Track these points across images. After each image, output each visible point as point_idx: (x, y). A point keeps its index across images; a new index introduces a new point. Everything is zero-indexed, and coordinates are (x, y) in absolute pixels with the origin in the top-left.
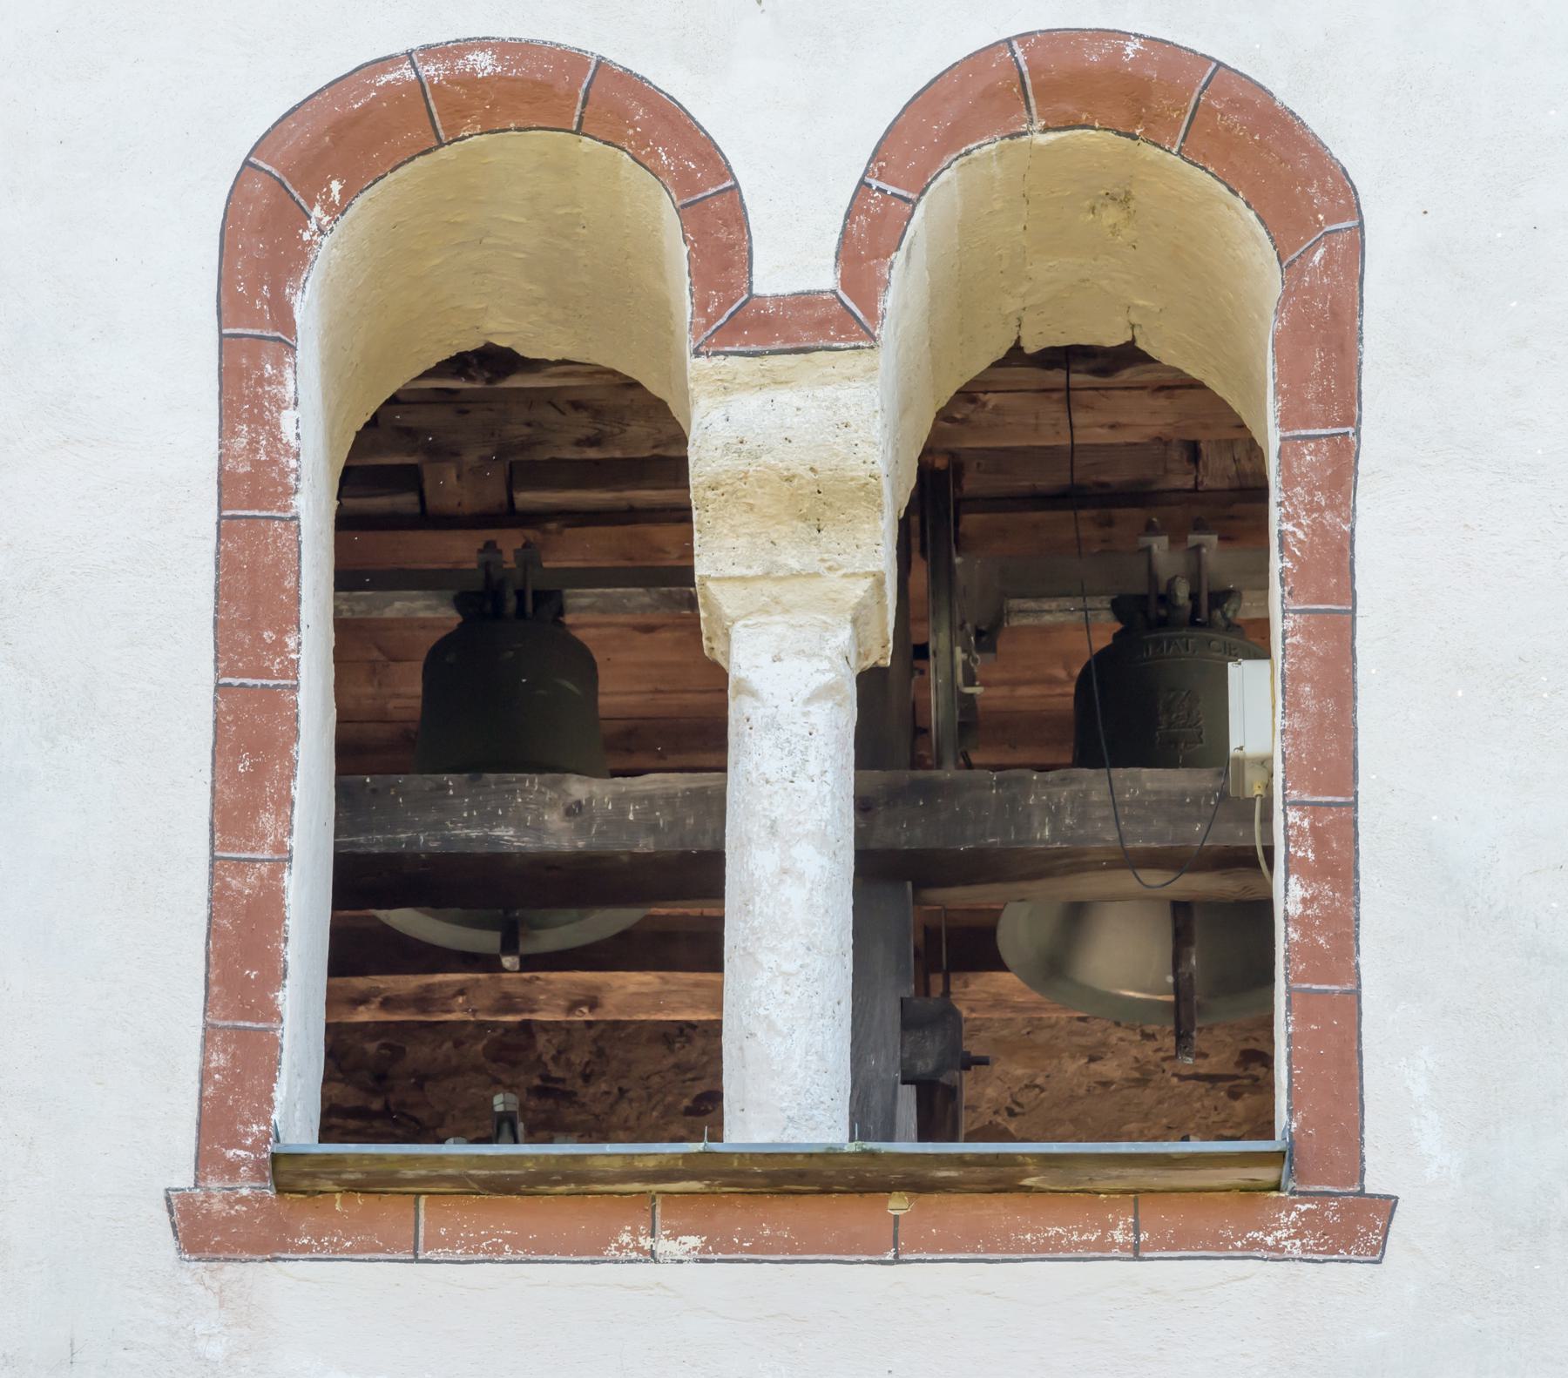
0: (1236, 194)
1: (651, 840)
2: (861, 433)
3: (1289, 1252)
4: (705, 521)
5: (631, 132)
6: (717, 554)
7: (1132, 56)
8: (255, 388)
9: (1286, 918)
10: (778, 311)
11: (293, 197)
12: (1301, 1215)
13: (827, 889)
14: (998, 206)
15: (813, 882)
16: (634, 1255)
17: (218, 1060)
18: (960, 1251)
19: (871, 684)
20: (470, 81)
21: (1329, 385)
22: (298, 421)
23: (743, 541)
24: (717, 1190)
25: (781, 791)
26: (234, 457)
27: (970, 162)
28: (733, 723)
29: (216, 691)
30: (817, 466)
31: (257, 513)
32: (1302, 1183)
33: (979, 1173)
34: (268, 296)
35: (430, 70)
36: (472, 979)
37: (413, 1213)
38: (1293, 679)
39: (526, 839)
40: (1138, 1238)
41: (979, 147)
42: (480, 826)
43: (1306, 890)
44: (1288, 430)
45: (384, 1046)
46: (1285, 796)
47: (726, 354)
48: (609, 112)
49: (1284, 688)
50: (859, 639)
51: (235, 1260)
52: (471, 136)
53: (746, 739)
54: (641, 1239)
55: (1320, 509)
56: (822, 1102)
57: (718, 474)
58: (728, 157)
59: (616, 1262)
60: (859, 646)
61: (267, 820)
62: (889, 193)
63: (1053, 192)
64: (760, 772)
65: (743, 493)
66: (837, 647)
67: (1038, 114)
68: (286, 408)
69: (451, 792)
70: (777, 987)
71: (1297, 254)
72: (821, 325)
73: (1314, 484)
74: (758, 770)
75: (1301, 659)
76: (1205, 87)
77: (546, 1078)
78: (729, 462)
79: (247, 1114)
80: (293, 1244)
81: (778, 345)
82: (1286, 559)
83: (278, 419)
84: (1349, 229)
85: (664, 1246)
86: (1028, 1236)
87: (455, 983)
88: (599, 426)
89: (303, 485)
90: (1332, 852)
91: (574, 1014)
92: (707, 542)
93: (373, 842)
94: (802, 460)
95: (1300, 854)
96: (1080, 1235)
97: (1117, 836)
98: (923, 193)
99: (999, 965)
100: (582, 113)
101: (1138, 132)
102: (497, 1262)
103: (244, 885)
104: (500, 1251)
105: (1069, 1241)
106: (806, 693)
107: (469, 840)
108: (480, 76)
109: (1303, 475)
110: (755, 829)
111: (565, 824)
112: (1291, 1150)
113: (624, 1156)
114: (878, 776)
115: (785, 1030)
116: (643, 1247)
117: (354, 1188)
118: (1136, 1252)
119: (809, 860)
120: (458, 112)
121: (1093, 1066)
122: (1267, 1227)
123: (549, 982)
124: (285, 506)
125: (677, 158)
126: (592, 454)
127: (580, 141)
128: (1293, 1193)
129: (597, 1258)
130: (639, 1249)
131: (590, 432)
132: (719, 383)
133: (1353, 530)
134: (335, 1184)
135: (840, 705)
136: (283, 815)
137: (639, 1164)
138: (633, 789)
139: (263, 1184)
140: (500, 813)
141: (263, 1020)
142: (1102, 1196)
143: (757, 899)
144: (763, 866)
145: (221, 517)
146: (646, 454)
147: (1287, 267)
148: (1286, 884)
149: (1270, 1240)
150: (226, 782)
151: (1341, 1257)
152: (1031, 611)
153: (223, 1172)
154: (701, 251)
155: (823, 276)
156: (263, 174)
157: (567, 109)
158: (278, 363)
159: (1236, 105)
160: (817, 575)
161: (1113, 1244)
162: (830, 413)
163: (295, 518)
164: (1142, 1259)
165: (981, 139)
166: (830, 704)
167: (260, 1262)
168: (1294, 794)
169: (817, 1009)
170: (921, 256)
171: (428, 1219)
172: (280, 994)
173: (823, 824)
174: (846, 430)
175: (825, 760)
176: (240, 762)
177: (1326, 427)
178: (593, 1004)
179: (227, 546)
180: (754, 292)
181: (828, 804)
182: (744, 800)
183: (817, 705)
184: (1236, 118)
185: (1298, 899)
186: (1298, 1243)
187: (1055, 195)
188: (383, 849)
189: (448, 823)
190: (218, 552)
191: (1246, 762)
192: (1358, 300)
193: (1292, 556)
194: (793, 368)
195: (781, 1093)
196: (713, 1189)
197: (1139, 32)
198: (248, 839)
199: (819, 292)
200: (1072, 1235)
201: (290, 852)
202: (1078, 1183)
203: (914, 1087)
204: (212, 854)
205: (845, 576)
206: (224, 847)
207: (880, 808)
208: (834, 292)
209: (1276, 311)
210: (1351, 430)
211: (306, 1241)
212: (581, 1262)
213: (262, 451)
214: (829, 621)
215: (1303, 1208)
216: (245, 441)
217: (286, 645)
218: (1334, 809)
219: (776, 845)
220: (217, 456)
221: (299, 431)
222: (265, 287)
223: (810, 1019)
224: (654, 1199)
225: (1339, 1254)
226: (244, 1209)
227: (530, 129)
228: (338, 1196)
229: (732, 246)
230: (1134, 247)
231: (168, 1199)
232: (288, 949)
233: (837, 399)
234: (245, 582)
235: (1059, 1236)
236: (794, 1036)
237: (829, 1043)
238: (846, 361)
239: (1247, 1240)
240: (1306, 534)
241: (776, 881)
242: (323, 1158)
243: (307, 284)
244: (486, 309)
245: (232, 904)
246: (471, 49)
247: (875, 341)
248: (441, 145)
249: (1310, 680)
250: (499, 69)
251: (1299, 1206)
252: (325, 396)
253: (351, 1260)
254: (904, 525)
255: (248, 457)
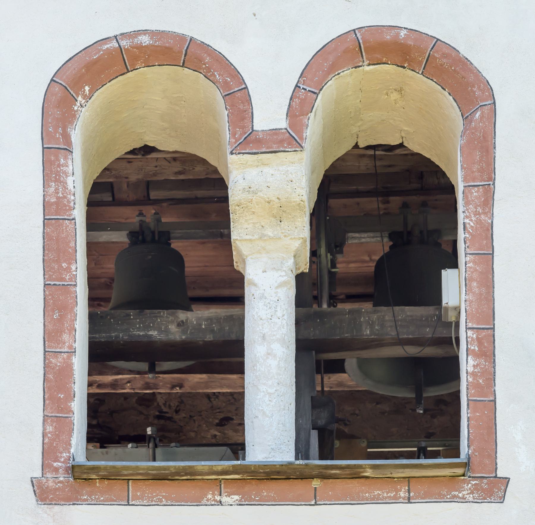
0: (445, 90)
1: (211, 336)
2: (297, 184)
3: (468, 499)
4: (235, 218)
5: (204, 66)
6: (240, 231)
7: (403, 36)
8: (57, 168)
9: (467, 373)
10: (264, 137)
11: (70, 93)
12: (472, 485)
13: (285, 360)
14: (350, 93)
15: (280, 358)
16: (213, 503)
17: (49, 429)
18: (341, 500)
19: (300, 278)
20: (140, 47)
21: (482, 165)
22: (74, 181)
23: (251, 225)
24: (245, 478)
25: (267, 323)
26: (49, 195)
27: (339, 77)
28: (247, 296)
29: (44, 286)
30: (280, 197)
31: (59, 217)
32: (473, 473)
33: (348, 472)
34: (61, 132)
35: (124, 43)
36: (133, 377)
37: (127, 487)
38: (469, 280)
39: (162, 335)
40: (409, 495)
41: (343, 72)
42: (144, 330)
43: (475, 362)
44: (467, 183)
45: (97, 399)
46: (466, 325)
47: (243, 153)
48: (195, 58)
49: (466, 284)
50: (296, 263)
51: (58, 504)
52: (140, 68)
53: (252, 302)
54: (216, 497)
55: (479, 214)
56: (284, 442)
57: (240, 200)
58: (243, 76)
59: (206, 505)
60: (296, 265)
61: (65, 337)
62: (307, 90)
63: (372, 88)
64: (258, 315)
65: (251, 207)
66: (288, 266)
67: (366, 58)
68: (69, 176)
69: (132, 317)
70: (267, 398)
71: (469, 114)
72: (281, 142)
73: (477, 204)
74: (257, 315)
75: (472, 272)
76: (432, 48)
77: (161, 412)
78: (245, 196)
79: (61, 449)
80: (81, 499)
81: (264, 150)
82: (466, 234)
83: (66, 180)
84: (490, 104)
85: (225, 499)
86: (367, 495)
87: (126, 379)
88: (185, 167)
89: (76, 206)
90: (485, 347)
91: (173, 390)
92: (236, 226)
93: (102, 337)
94: (274, 194)
95: (472, 348)
96: (387, 494)
97: (396, 333)
98: (321, 90)
99: (344, 371)
100: (184, 59)
101: (406, 65)
102: (160, 505)
103: (57, 362)
104: (161, 501)
105: (383, 496)
106: (276, 285)
107: (139, 336)
108: (144, 45)
109: (473, 201)
110: (257, 338)
111: (177, 330)
112: (469, 463)
113: (209, 466)
114: (302, 310)
115: (270, 415)
116: (217, 500)
117: (103, 478)
118: (409, 501)
119: (278, 350)
120: (135, 59)
121: (378, 406)
122: (460, 490)
123: (164, 378)
124: (70, 214)
125: (222, 76)
126: (182, 177)
127: (184, 70)
128: (470, 477)
129: (199, 504)
130: (215, 500)
131: (180, 169)
132: (241, 165)
133: (492, 222)
134: (96, 476)
135: (289, 289)
136: (72, 335)
137: (215, 469)
138: (204, 316)
139: (68, 476)
140: (151, 325)
141: (66, 413)
142: (396, 479)
143: (258, 364)
144: (260, 352)
145: (45, 219)
146: (203, 177)
147: (465, 118)
148: (467, 360)
149: (460, 495)
150: (49, 322)
151: (488, 501)
152: (357, 238)
153: (53, 471)
154: (233, 113)
155: (283, 124)
156: (58, 84)
157: (178, 57)
158: (66, 158)
159: (445, 56)
160: (280, 238)
161: (400, 497)
162: (285, 176)
163: (74, 219)
164: (411, 503)
165: (344, 69)
166: (285, 289)
167: (68, 505)
168: (470, 325)
169: (282, 407)
170: (320, 114)
171: (133, 490)
172: (73, 404)
173: (284, 335)
174: (291, 183)
175: (284, 311)
176: (55, 314)
177: (481, 182)
178: (181, 386)
179: (47, 230)
180: (254, 129)
181: (285, 327)
182: (252, 326)
183: (280, 289)
184: (445, 60)
185: (472, 365)
186: (471, 496)
187: (372, 89)
188: (106, 340)
189: (131, 329)
190: (44, 233)
191: (449, 309)
192: (493, 133)
193: (469, 232)
194: (270, 159)
195: (269, 439)
196: (244, 478)
197: (406, 27)
198: (58, 344)
199: (280, 129)
200: (384, 494)
201: (75, 349)
202: (386, 475)
203: (317, 431)
204: (45, 350)
205: (291, 239)
206: (50, 347)
207: (302, 323)
208: (286, 129)
209: (461, 136)
210: (491, 183)
211: (86, 497)
212: (193, 505)
213: (60, 193)
214: (285, 256)
215: (473, 483)
216: (54, 189)
217: (71, 269)
218: (486, 331)
219: (265, 344)
220: (43, 195)
221: (75, 185)
222: (60, 129)
223: (279, 411)
224: (221, 482)
225: (487, 500)
226: (61, 485)
227: (164, 65)
228: (98, 480)
229: (245, 111)
230: (404, 108)
231: (32, 481)
232: (75, 386)
233: (288, 171)
234: (55, 244)
235: (379, 495)
236: (273, 417)
237: (287, 420)
238: (290, 156)
239: (452, 495)
240: (474, 224)
241: (265, 358)
242: (91, 467)
243: (76, 127)
244: (145, 132)
245: (53, 369)
246: (140, 35)
247: (303, 148)
248: (128, 71)
249: (476, 280)
250: (151, 42)
251: (472, 482)
252: (83, 168)
253: (103, 504)
254: (312, 215)
255: (54, 195)
